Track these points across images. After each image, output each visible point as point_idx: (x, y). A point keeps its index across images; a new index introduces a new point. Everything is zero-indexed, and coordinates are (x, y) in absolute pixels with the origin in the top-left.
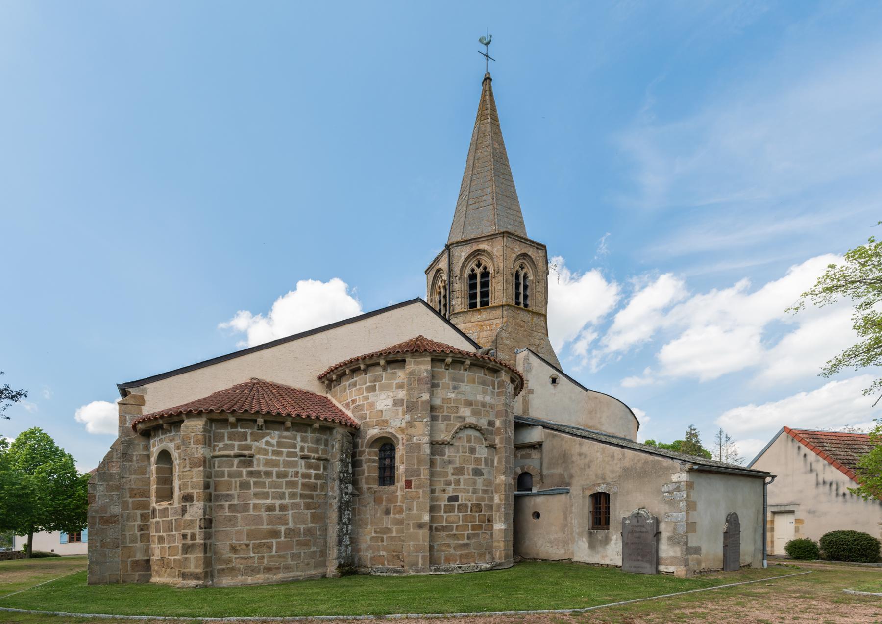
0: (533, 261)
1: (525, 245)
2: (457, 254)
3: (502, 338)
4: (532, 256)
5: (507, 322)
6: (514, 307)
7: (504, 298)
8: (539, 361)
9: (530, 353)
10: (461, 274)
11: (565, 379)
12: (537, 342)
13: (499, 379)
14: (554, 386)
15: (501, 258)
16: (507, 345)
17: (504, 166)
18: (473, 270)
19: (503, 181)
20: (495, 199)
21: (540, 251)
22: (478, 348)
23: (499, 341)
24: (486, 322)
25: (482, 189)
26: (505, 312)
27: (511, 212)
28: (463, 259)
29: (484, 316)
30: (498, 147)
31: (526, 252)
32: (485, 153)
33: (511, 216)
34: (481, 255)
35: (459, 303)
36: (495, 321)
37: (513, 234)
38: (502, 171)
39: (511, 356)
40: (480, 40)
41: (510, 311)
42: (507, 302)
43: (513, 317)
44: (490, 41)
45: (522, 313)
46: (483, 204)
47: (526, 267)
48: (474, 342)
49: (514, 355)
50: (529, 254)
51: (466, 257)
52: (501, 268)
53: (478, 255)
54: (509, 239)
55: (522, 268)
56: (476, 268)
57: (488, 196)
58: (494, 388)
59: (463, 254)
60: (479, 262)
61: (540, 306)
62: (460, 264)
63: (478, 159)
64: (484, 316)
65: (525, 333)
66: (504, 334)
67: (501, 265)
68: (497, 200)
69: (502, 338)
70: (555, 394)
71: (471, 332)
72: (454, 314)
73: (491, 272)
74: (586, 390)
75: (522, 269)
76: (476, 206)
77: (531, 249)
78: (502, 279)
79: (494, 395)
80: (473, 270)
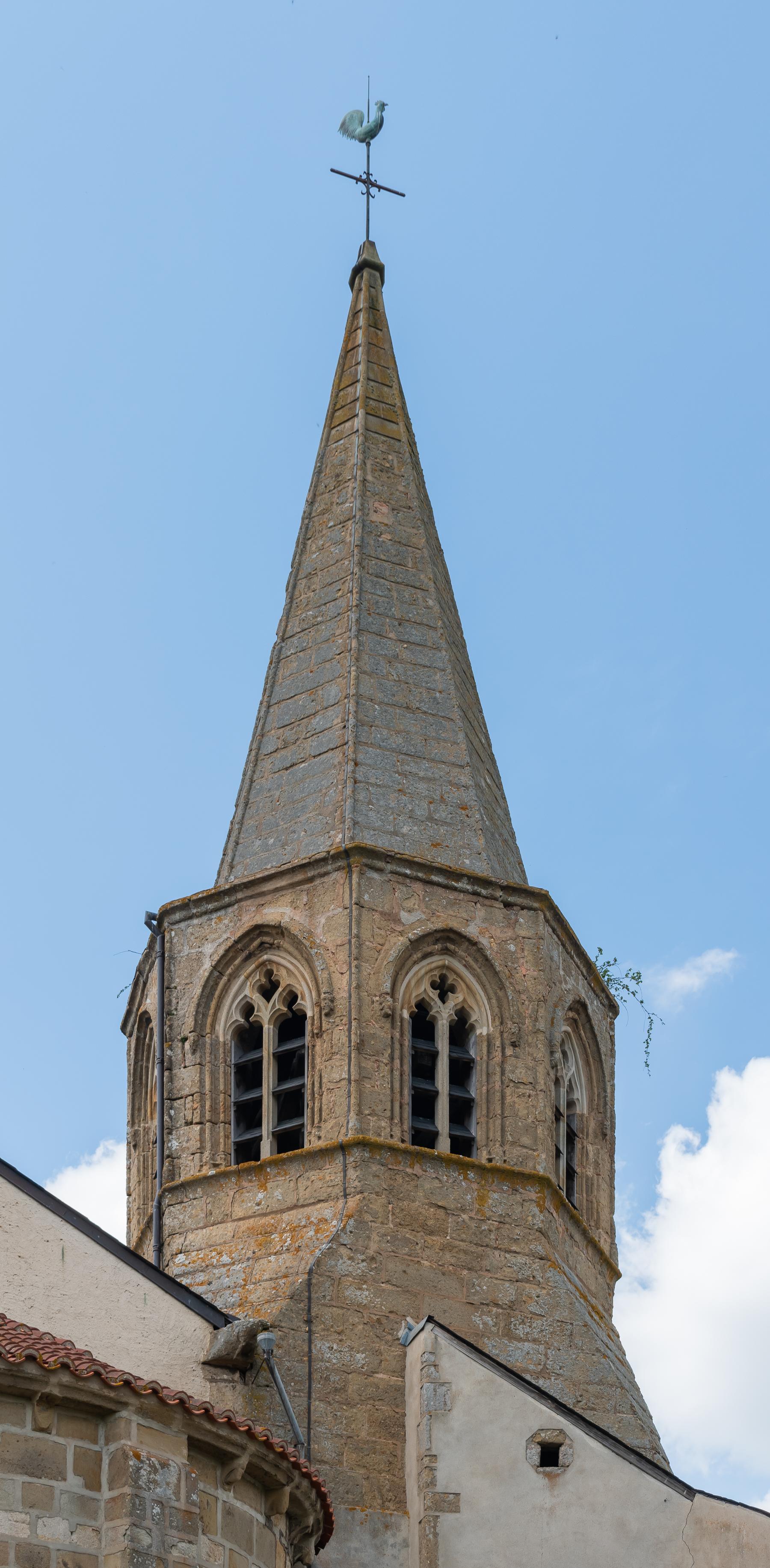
0: (487, 959)
1: (452, 896)
2: (186, 950)
3: (337, 1282)
4: (484, 941)
5: (360, 1212)
6: (405, 1152)
7: (352, 1114)
8: (481, 1371)
9: (444, 1339)
10: (199, 1028)
11: (593, 1444)
12: (507, 1293)
13: (113, 1447)
14: (548, 1475)
15: (342, 955)
16: (359, 1309)
17: (407, 593)
18: (248, 1010)
19: (399, 649)
20: (352, 721)
21: (523, 918)
22: (219, 1321)
23: (324, 1290)
24: (286, 1216)
25: (312, 691)
26: (352, 1174)
27: (422, 769)
28: (207, 965)
29: (278, 1194)
30: (389, 521)
31: (455, 924)
32: (335, 550)
33: (422, 786)
34: (271, 946)
35: (194, 1144)
36: (314, 1213)
37: (388, 857)
38: (396, 612)
39: (378, 1353)
40: (345, 129)
41: (375, 1168)
42: (360, 1130)
43: (390, 1190)
44: (379, 125)
45: (431, 1172)
46: (311, 746)
47: (460, 986)
48: (198, 1297)
49: (396, 1351)
50: (471, 931)
51: (216, 958)
52: (342, 994)
53: (262, 947)
54: (375, 875)
55: (443, 988)
56: (257, 999)
57: (330, 712)
58: (93, 1484)
59: (208, 948)
60: (269, 973)
61: (526, 1140)
62: (197, 990)
63: (309, 576)
64: (278, 1194)
65: (448, 1257)
66: (343, 1265)
67: (342, 984)
68: (359, 724)
69: (337, 1282)
70: (552, 1510)
71: (225, 1259)
72: (172, 1190)
73: (309, 1014)
74: (690, 1492)
75: (443, 998)
76: (288, 755)
77: (480, 912)
78: (345, 1039)
79: (94, 1515)
80: (248, 1010)
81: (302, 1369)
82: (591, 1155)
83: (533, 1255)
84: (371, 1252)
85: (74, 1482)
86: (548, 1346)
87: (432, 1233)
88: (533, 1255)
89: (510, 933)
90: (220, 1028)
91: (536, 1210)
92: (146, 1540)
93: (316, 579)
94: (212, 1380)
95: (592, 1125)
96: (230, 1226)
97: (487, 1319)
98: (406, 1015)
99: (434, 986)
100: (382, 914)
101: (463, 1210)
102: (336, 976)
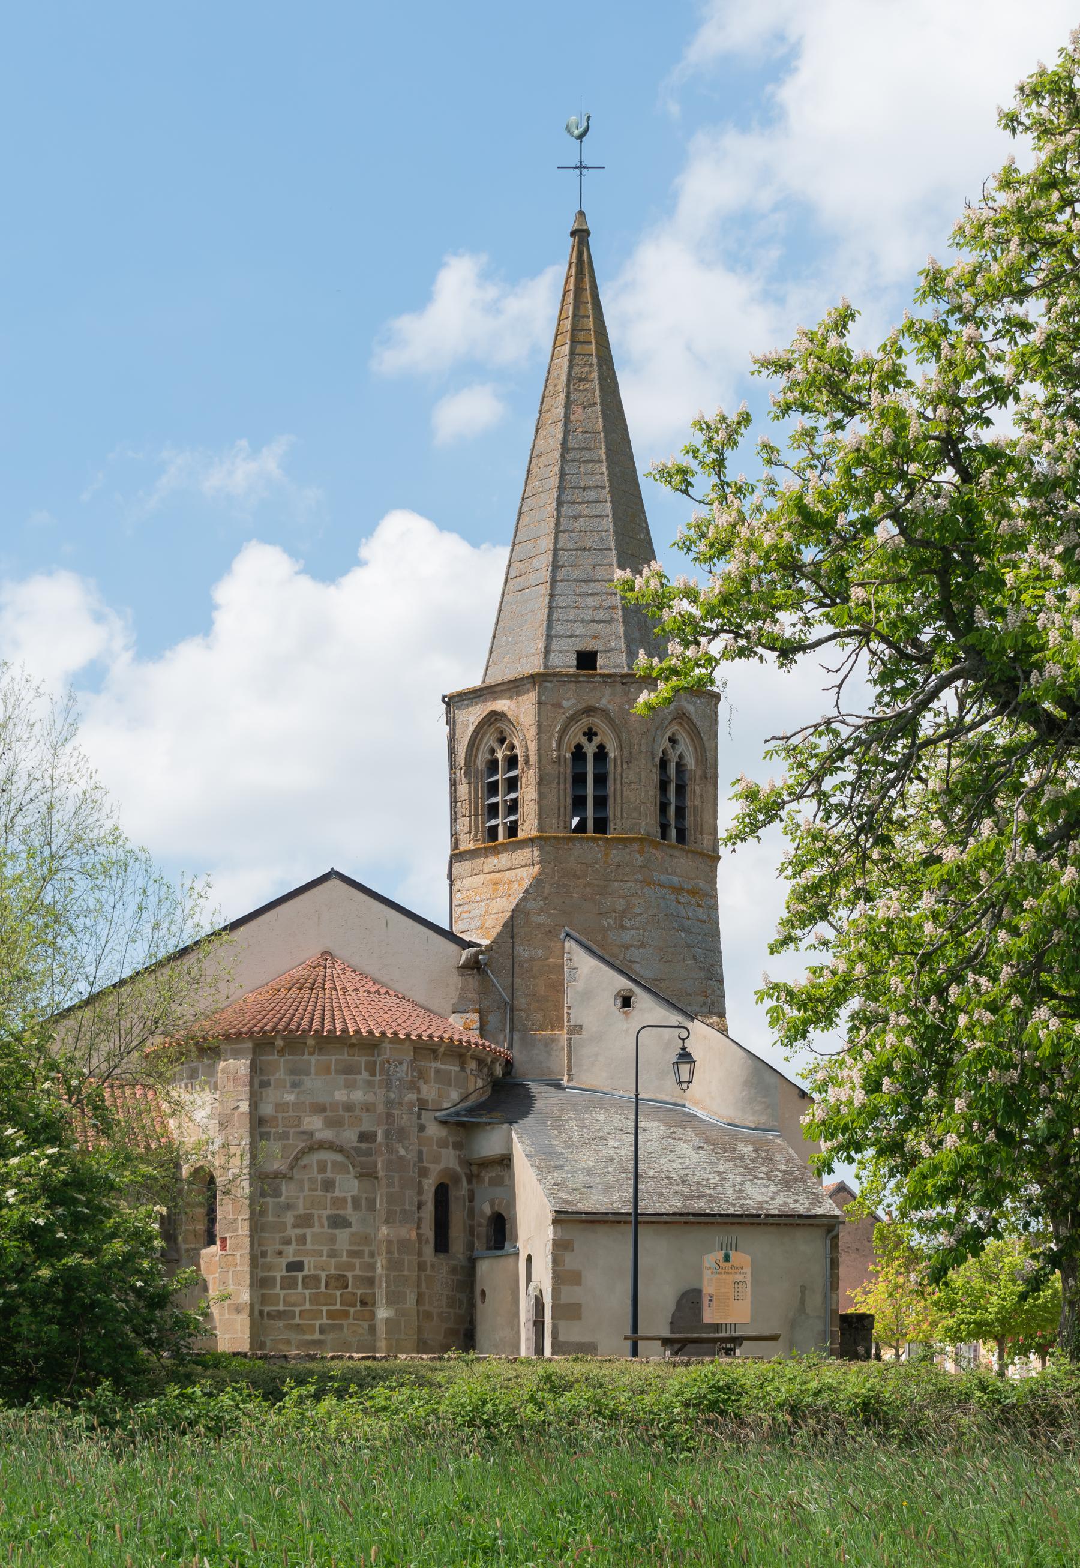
14: (625, 1013)
16: (540, 926)
17: (589, 467)
25: (535, 539)
28: (471, 728)
31: (593, 703)
35: (466, 828)
50: (604, 703)
54: (549, 684)
56: (496, 745)
58: (373, 1074)
59: (472, 719)
60: (502, 732)
64: (503, 860)
65: (588, 889)
75: (590, 740)
81: (509, 963)
82: (698, 792)
83: (636, 881)
84: (545, 895)
85: (365, 1075)
86: (644, 930)
87: (579, 878)
88: (636, 881)
89: (626, 699)
90: (479, 761)
91: (638, 855)
92: (393, 1096)
93: (541, 459)
94: (462, 975)
95: (699, 773)
96: (482, 876)
97: (610, 921)
98: (568, 755)
99: (585, 734)
100: (552, 705)
101: (596, 863)
102: (529, 743)
